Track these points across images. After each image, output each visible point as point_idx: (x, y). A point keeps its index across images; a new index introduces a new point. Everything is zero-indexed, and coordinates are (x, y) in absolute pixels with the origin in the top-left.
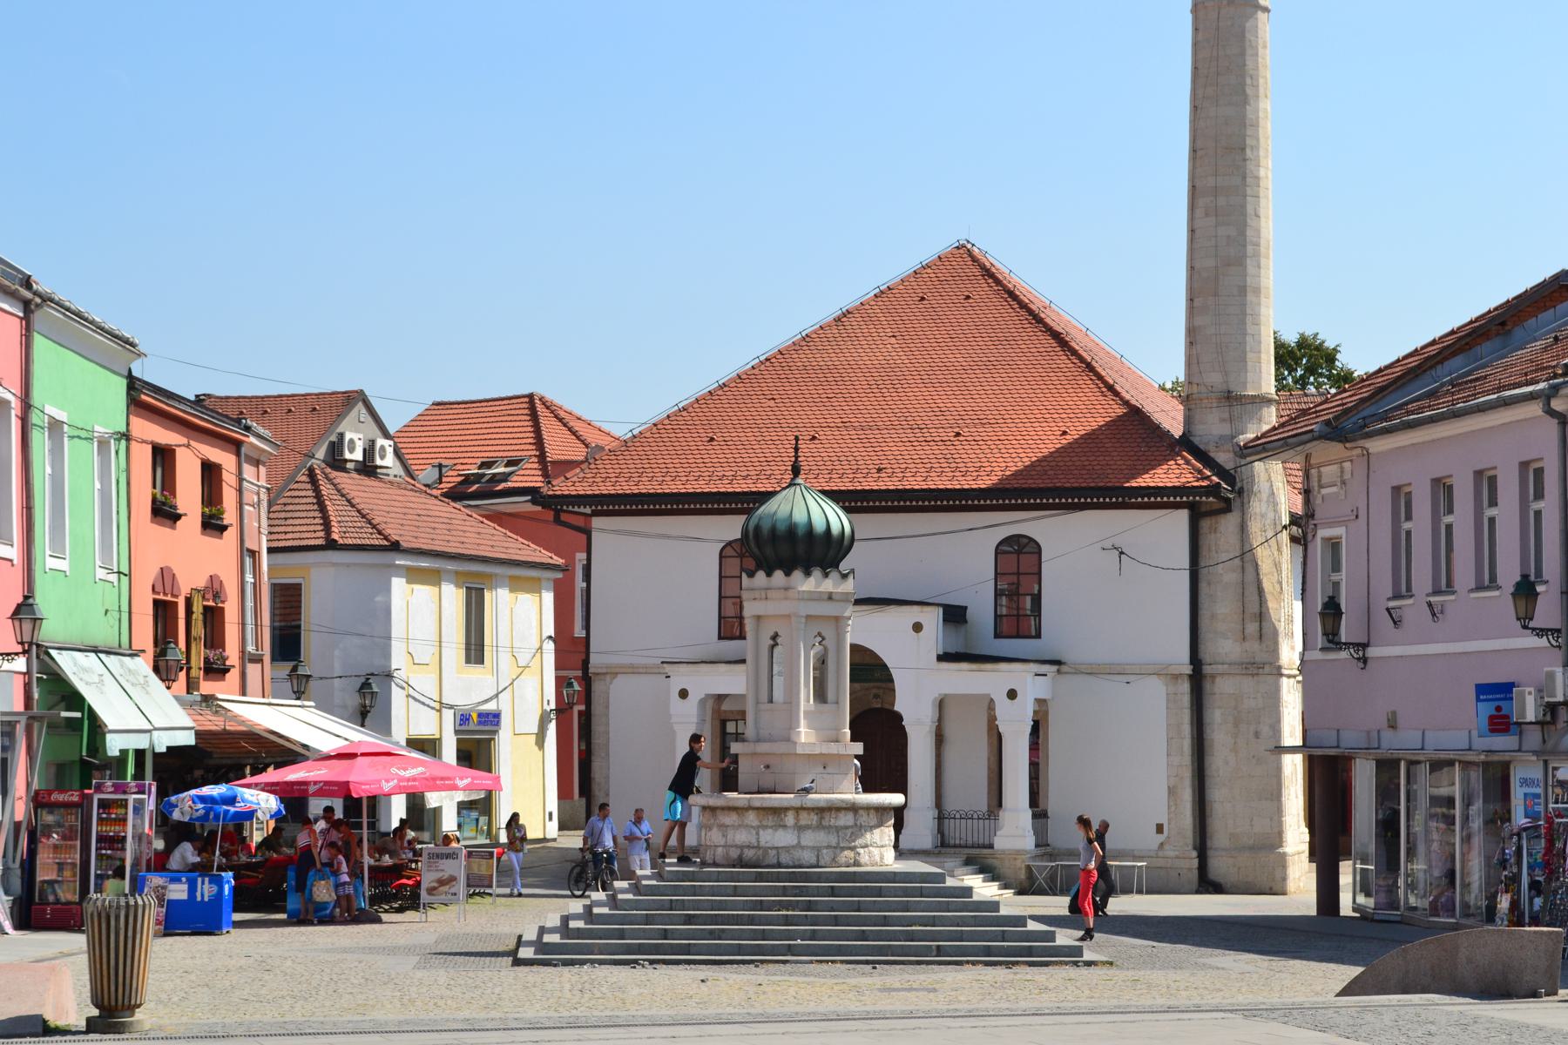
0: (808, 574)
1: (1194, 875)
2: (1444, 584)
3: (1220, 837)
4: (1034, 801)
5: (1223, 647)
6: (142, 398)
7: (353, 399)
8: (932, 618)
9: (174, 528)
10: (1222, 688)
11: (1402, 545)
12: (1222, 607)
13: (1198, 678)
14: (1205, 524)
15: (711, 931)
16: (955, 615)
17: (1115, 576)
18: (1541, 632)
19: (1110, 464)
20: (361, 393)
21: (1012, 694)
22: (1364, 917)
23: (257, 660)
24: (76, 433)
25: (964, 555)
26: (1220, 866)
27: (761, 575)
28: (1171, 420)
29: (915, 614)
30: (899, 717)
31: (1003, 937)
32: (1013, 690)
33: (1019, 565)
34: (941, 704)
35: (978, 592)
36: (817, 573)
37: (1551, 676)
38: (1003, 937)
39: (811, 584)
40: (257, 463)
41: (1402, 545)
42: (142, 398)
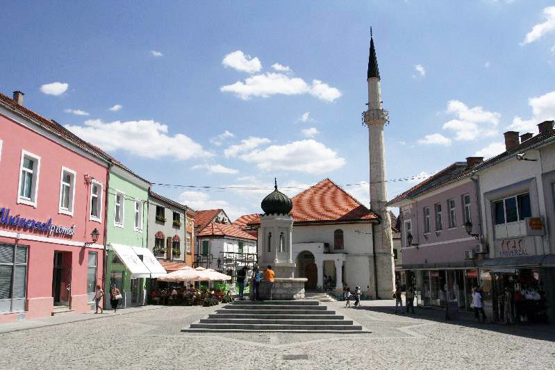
0: (279, 214)
1: (375, 296)
2: (439, 227)
3: (379, 289)
4: (343, 281)
5: (379, 250)
6: (152, 196)
7: (220, 211)
8: (322, 245)
9: (164, 225)
10: (380, 258)
11: (427, 222)
12: (379, 243)
13: (375, 257)
14: (376, 227)
15: (205, 325)
16: (326, 245)
17: (359, 240)
18: (473, 235)
19: (357, 215)
20: (222, 210)
21: (338, 260)
22: (419, 306)
23: (190, 254)
24: (127, 197)
25: (328, 234)
26: (380, 294)
27: (270, 215)
28: (368, 207)
29: (320, 244)
30: (316, 265)
31: (336, 323)
32: (338, 259)
33: (339, 236)
34: (324, 262)
35: (331, 240)
36: (281, 215)
37: (478, 246)
38: (336, 323)
39: (279, 218)
40: (191, 217)
41: (427, 222)
42: (152, 196)
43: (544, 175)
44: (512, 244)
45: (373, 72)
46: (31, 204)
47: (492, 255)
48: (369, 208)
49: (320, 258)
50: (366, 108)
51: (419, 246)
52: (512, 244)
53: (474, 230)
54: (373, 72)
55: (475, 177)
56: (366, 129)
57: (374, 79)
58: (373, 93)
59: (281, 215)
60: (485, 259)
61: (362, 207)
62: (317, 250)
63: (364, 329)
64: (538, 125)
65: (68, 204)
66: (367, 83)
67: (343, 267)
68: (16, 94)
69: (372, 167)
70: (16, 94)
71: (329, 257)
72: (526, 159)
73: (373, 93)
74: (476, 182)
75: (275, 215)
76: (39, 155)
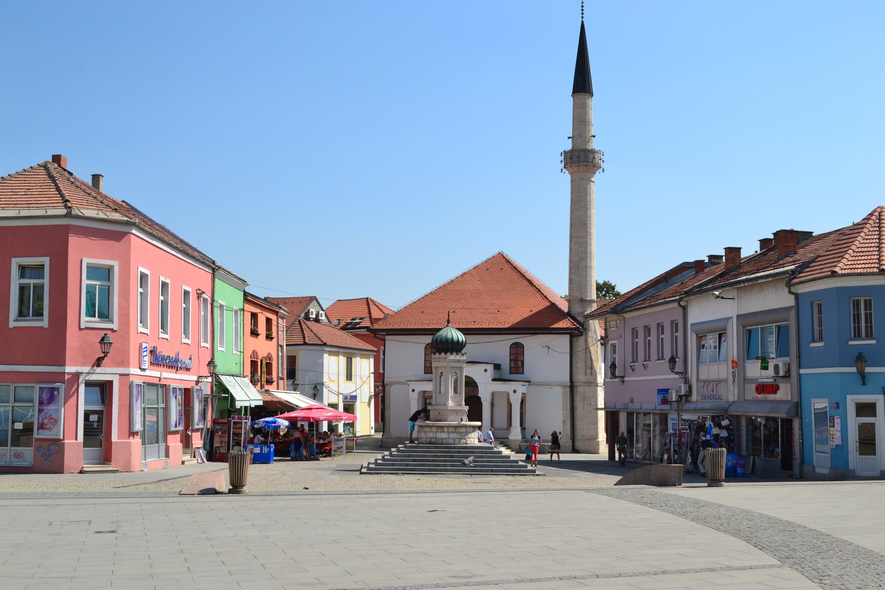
1: (571, 448)
2: (648, 358)
3: (579, 436)
5: (580, 377)
7: (313, 299)
8: (490, 368)
10: (580, 390)
12: (579, 365)
13: (572, 387)
14: (575, 339)
16: (497, 367)
17: (546, 356)
18: (677, 373)
19: (546, 320)
21: (515, 391)
25: (501, 348)
26: (579, 445)
29: (485, 366)
30: (480, 398)
32: (515, 390)
33: (517, 351)
34: (493, 394)
37: (680, 387)
40: (283, 318)
41: (635, 346)
42: (248, 298)
43: (739, 317)
44: (710, 387)
45: (582, 83)
46: (109, 326)
47: (694, 397)
48: (566, 310)
49: (486, 389)
50: (568, 146)
51: (626, 379)
52: (710, 387)
53: (679, 367)
54: (582, 83)
55: (682, 303)
56: (567, 177)
57: (581, 96)
58: (581, 121)
59: (455, 354)
60: (687, 401)
61: (553, 306)
62: (482, 376)
63: (537, 473)
64: (760, 241)
65: (143, 321)
66: (571, 100)
67: (522, 402)
68: (96, 178)
69: (574, 240)
70: (96, 178)
71: (500, 387)
72: (722, 298)
73: (581, 121)
74: (685, 309)
75: (449, 354)
76: (112, 259)
